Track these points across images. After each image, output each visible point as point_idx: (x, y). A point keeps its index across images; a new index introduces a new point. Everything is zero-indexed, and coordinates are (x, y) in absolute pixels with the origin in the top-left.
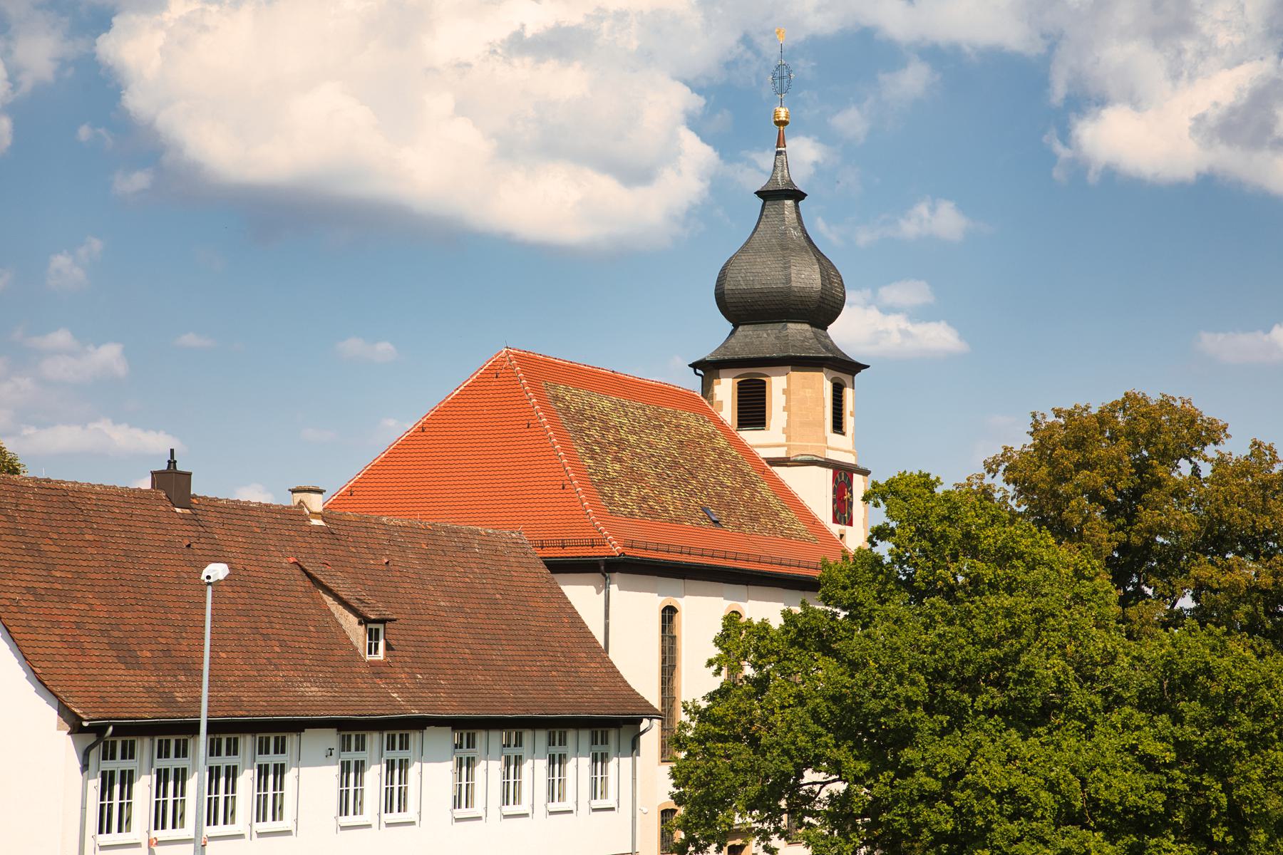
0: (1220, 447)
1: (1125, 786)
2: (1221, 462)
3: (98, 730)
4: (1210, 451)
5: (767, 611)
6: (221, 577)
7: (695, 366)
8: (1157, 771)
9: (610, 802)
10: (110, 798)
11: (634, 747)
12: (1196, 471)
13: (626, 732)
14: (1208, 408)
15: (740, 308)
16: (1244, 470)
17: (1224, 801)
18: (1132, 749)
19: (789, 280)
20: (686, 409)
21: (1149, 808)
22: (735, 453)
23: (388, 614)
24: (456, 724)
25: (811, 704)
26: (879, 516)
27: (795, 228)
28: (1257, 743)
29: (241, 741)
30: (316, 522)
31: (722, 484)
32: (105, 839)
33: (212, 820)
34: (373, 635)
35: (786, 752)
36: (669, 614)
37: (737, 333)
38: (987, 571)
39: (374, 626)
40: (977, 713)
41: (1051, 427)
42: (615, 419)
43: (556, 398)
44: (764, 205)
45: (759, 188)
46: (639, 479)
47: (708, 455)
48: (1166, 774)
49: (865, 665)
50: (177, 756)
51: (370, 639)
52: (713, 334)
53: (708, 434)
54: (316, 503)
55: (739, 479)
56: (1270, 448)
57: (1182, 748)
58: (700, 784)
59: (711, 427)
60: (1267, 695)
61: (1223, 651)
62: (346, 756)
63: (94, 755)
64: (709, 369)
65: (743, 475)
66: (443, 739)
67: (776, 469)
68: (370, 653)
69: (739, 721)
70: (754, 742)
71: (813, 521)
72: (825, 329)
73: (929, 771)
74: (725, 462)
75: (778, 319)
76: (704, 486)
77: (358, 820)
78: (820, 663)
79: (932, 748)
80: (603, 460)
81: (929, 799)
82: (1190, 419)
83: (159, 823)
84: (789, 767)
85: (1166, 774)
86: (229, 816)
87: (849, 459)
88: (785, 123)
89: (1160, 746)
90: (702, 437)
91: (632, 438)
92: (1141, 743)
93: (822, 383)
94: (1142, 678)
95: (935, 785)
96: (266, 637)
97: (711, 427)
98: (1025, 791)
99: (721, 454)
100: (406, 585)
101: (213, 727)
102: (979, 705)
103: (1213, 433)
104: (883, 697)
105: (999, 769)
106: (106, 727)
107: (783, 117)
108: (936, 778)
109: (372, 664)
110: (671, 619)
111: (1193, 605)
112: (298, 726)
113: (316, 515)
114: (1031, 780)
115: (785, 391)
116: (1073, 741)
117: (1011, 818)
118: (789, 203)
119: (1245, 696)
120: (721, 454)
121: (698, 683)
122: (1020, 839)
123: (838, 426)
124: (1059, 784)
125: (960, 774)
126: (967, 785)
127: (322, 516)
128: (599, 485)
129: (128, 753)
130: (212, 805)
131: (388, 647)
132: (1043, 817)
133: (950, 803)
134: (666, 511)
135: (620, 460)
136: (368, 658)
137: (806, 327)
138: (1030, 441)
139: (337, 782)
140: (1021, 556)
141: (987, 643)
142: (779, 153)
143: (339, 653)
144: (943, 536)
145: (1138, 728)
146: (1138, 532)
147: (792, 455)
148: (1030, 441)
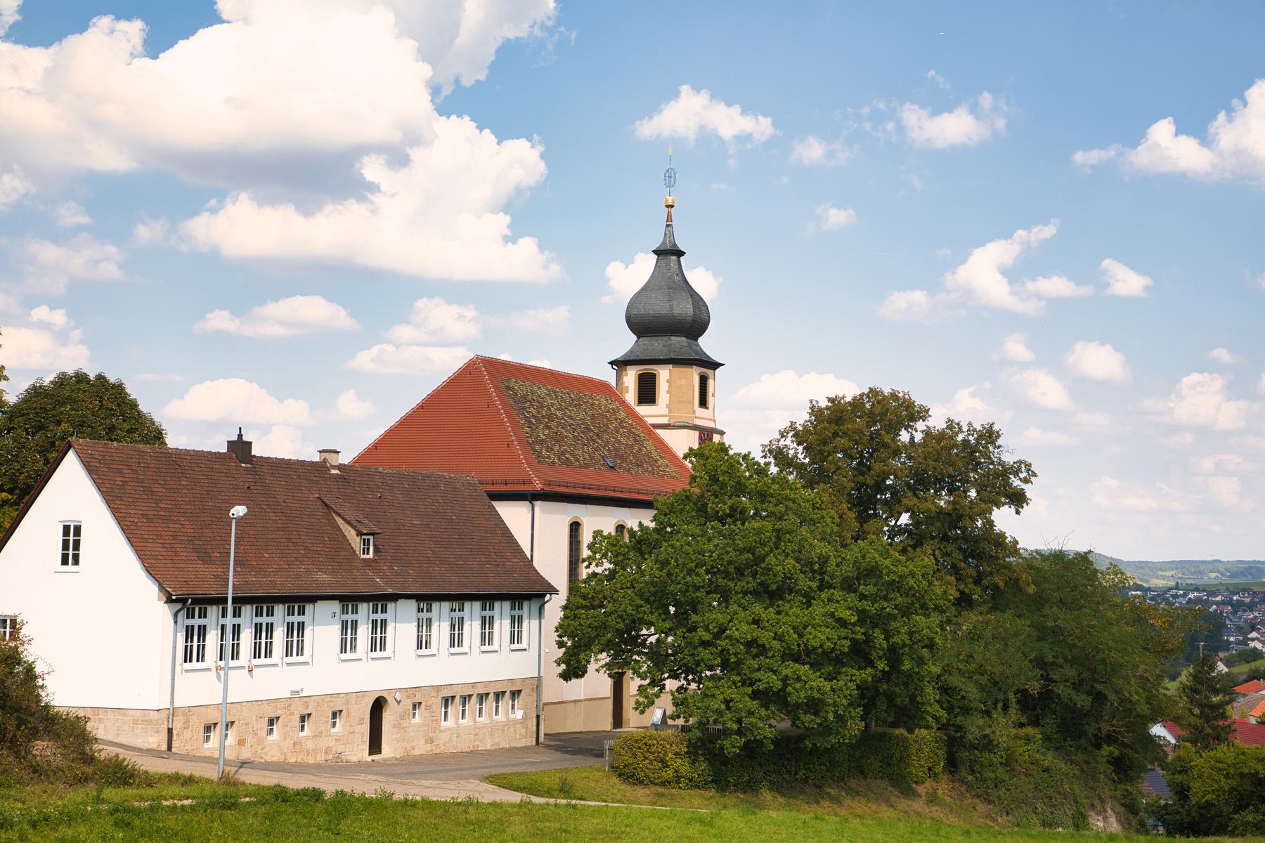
1: (820, 637)
2: (928, 433)
3: (184, 601)
4: (920, 425)
7: (612, 363)
9: (524, 645)
12: (912, 438)
14: (919, 399)
15: (641, 325)
16: (941, 436)
19: (671, 308)
23: (376, 530)
24: (419, 598)
28: (906, 612)
30: (333, 471)
31: (619, 442)
32: (188, 666)
33: (373, 649)
35: (620, 617)
36: (575, 527)
40: (737, 593)
42: (548, 401)
43: (508, 388)
57: (862, 613)
59: (616, 405)
64: (620, 365)
65: (635, 435)
73: (707, 629)
75: (670, 331)
76: (607, 444)
81: (705, 644)
82: (908, 404)
83: (257, 654)
86: (269, 653)
87: (710, 425)
91: (559, 414)
93: (694, 374)
94: (848, 570)
95: (707, 637)
96: (295, 544)
97: (616, 405)
98: (762, 640)
101: (235, 600)
102: (738, 588)
103: (923, 414)
106: (186, 600)
112: (313, 599)
118: (674, 258)
122: (759, 669)
125: (724, 631)
129: (203, 614)
131: (376, 550)
134: (578, 460)
135: (549, 428)
137: (684, 339)
139: (339, 632)
147: (672, 422)
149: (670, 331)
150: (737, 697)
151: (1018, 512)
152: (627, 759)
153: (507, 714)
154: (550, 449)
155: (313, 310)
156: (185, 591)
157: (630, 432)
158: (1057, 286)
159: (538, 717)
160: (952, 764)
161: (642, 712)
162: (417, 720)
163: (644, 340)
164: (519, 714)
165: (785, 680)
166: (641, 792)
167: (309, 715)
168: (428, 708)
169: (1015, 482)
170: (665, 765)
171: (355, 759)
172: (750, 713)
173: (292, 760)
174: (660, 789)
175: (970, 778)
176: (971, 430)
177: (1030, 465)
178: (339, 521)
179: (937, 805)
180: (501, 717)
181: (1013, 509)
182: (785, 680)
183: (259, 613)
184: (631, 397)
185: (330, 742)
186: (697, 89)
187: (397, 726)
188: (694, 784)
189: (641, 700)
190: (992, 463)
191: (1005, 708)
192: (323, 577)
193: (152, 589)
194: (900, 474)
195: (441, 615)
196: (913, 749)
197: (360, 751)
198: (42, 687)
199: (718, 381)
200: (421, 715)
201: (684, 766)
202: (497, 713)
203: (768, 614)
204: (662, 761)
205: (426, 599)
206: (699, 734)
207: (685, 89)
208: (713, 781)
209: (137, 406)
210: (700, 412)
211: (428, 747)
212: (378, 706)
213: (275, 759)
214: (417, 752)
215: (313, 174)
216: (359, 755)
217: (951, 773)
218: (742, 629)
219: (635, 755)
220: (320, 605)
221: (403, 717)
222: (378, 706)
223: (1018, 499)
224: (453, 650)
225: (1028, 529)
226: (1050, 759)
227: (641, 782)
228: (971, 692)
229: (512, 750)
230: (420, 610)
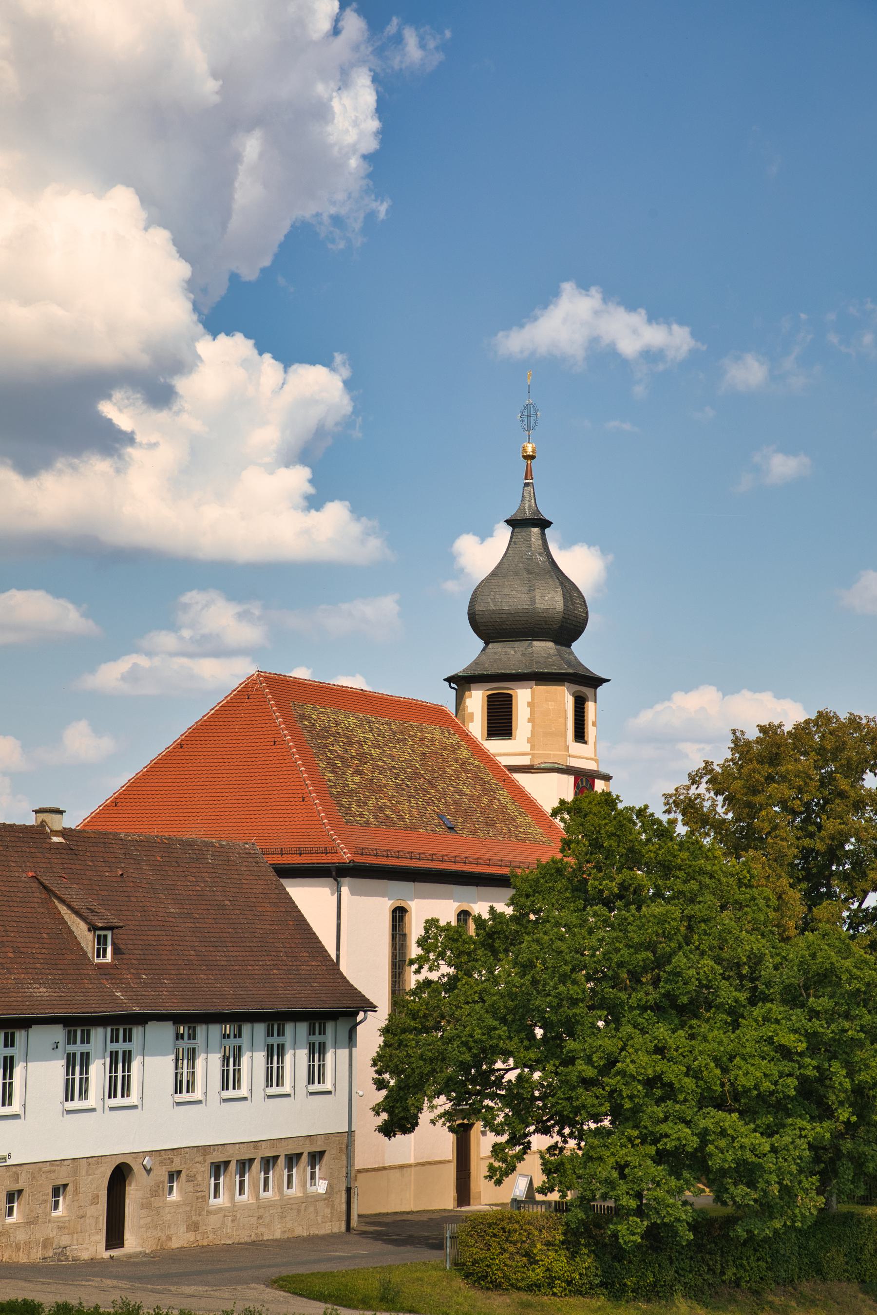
1: (755, 1073)
7: (449, 680)
9: (328, 1086)
11: (351, 1040)
13: (343, 1027)
15: (489, 627)
17: (848, 1085)
18: (770, 1041)
19: (533, 602)
20: (432, 723)
21: (783, 1092)
22: (477, 763)
23: (115, 922)
24: (177, 1019)
27: (540, 554)
30: (55, 839)
31: (461, 793)
33: (112, 1094)
34: (101, 941)
35: (465, 1044)
36: (399, 915)
37: (488, 650)
39: (102, 933)
40: (631, 1008)
42: (360, 735)
43: (303, 717)
44: (512, 533)
45: (508, 518)
47: (451, 765)
48: (798, 1062)
51: (99, 944)
52: (468, 649)
53: (452, 745)
55: (478, 787)
62: (71, 1049)
64: (462, 683)
65: (483, 783)
66: (164, 1032)
68: (98, 956)
69: (431, 1015)
72: (569, 646)
73: (589, 1061)
76: (443, 795)
77: (126, 1102)
80: (344, 773)
81: (587, 1083)
85: (798, 1062)
86: (84, 1093)
87: (590, 766)
88: (532, 457)
89: (793, 1037)
90: (445, 749)
91: (375, 752)
92: (777, 1035)
94: (791, 975)
95: (590, 1072)
99: (464, 763)
100: (138, 894)
102: (633, 1002)
107: (529, 451)
109: (100, 966)
110: (402, 919)
114: (674, 1067)
115: (529, 704)
117: (659, 1101)
118: (536, 530)
119: (865, 993)
123: (580, 735)
124: (702, 1072)
131: (116, 951)
132: (686, 1100)
134: (402, 819)
136: (96, 961)
139: (63, 1071)
142: (527, 485)
143: (70, 957)
146: (822, 839)
147: (536, 763)
150: (634, 1160)
152: (477, 1251)
153: (304, 1185)
154: (362, 804)
157: (476, 778)
159: (349, 1190)
161: (499, 1182)
162: (175, 1196)
164: (321, 1187)
165: (703, 1136)
167: (20, 1192)
168: (191, 1179)
170: (532, 1260)
171: (85, 1256)
174: (526, 1297)
180: (295, 1191)
182: (703, 1136)
184: (477, 727)
185: (50, 1231)
186: (584, 286)
188: (574, 1289)
189: (497, 1164)
192: (41, 991)
197: (93, 1246)
204: (527, 1254)
207: (568, 287)
210: (576, 748)
211: (191, 1237)
212: (120, 1175)
214: (175, 1244)
218: (639, 1062)
219: (488, 1247)
221: (155, 1192)
222: (120, 1175)
224: (227, 1094)
227: (497, 1286)
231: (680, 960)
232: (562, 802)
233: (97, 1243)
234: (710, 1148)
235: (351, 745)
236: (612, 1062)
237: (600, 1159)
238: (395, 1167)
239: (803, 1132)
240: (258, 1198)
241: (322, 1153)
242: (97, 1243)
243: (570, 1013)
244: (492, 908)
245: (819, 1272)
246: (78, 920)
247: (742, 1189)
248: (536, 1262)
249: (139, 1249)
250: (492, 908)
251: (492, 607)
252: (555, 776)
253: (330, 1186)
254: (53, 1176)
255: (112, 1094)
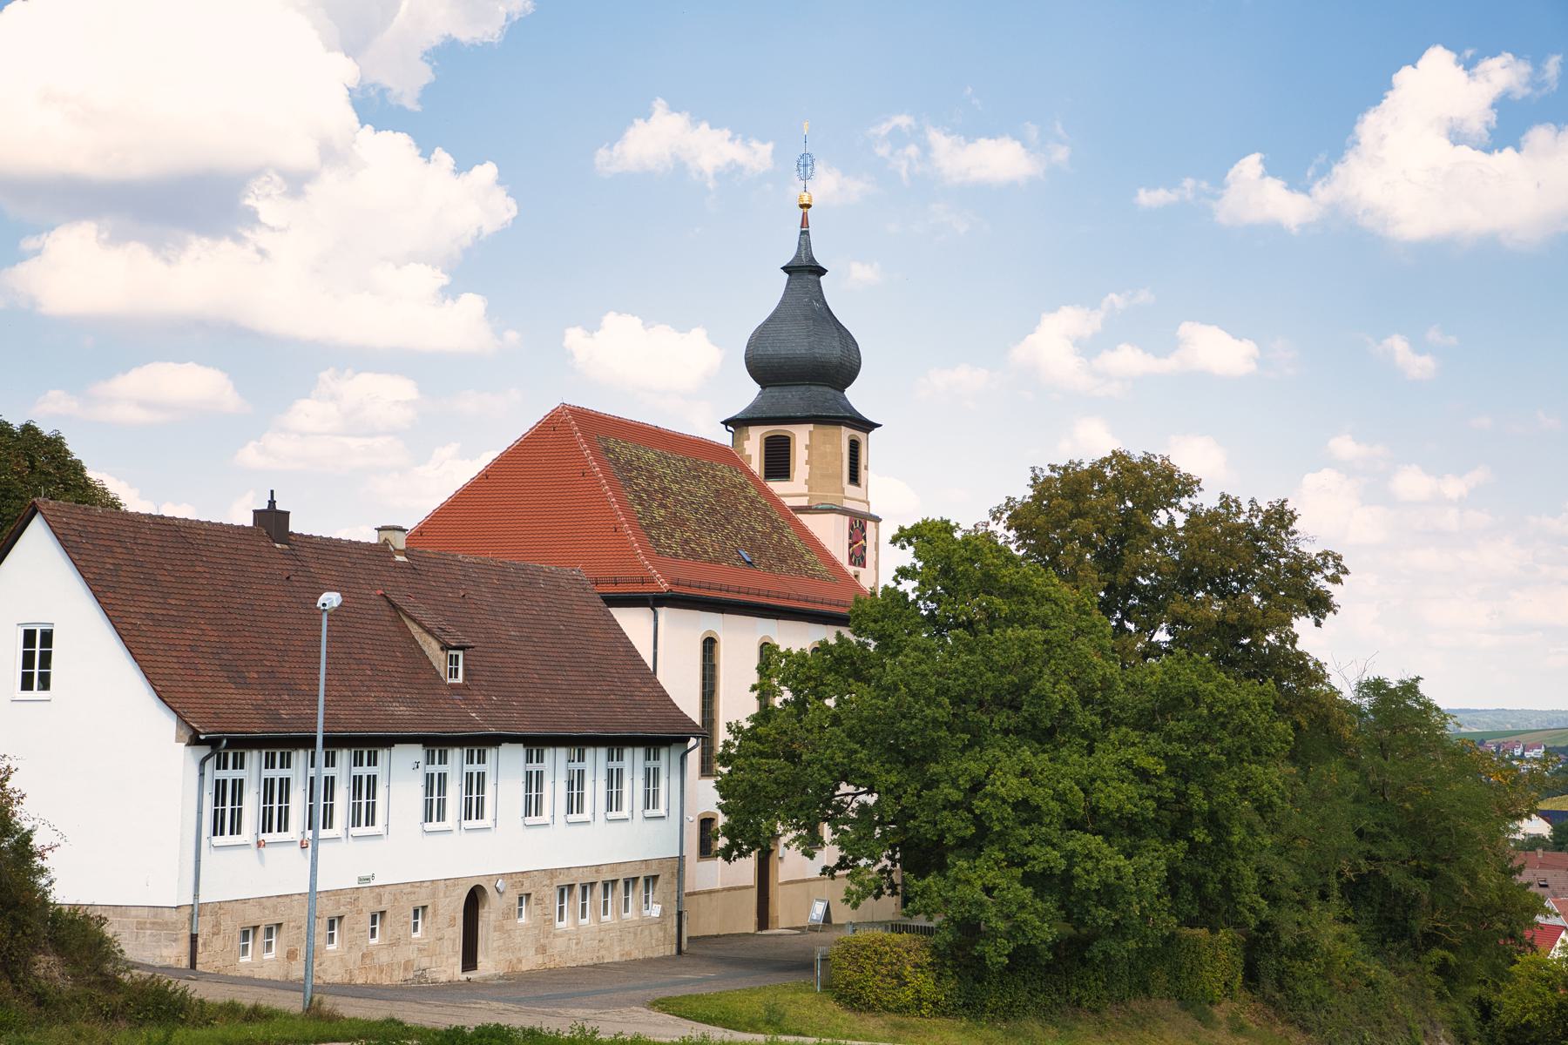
0: (1194, 500)
1: (1119, 796)
2: (1193, 514)
4: (1185, 502)
5: (798, 638)
6: (335, 605)
7: (726, 423)
8: (1148, 782)
9: (662, 811)
10: (223, 804)
12: (1171, 521)
14: (1186, 461)
15: (763, 369)
16: (1213, 517)
23: (467, 642)
25: (847, 724)
26: (906, 557)
28: (1234, 756)
29: (338, 754)
30: (399, 558)
31: (753, 529)
32: (218, 840)
35: (826, 767)
36: (709, 645)
38: (1003, 606)
39: (454, 653)
40: (995, 732)
41: (1048, 480)
43: (607, 450)
46: (681, 523)
49: (897, 689)
50: (235, 767)
54: (399, 541)
56: (1235, 501)
58: (744, 797)
59: (742, 478)
60: (1246, 716)
61: (1208, 677)
62: (431, 769)
63: (210, 764)
64: (736, 424)
65: (772, 521)
67: (800, 516)
70: (792, 757)
71: (833, 563)
73: (954, 783)
74: (756, 509)
75: (805, 373)
76: (739, 531)
78: (854, 688)
79: (955, 764)
81: (953, 806)
83: (267, 827)
84: (828, 780)
86: (441, 817)
87: (861, 508)
88: (809, 206)
89: (1152, 760)
91: (675, 487)
93: (846, 433)
95: (956, 796)
103: (1188, 486)
104: (914, 717)
105: (1015, 781)
106: (219, 741)
108: (958, 788)
109: (451, 685)
111: (1168, 638)
112: (389, 742)
113: (400, 552)
115: (807, 447)
116: (1076, 756)
120: (752, 502)
121: (737, 704)
122: (1031, 843)
126: (986, 795)
127: (404, 553)
128: (646, 528)
130: (356, 809)
133: (971, 811)
134: (706, 552)
136: (449, 681)
138: (1030, 492)
140: (1033, 594)
141: (1005, 670)
144: (965, 574)
145: (1134, 744)
147: (814, 504)
148: (1030, 492)
149: (805, 373)
150: (1003, 883)
151: (1318, 624)
152: (850, 973)
153: (640, 910)
154: (670, 536)
155: (191, 383)
156: (217, 727)
157: (766, 517)
158: (1128, 359)
159: (680, 914)
160: (1252, 976)
161: (855, 906)
162: (523, 920)
163: (775, 392)
164: (655, 911)
165: (1070, 856)
166: (871, 1023)
167: (340, 918)
168: (539, 901)
169: (1319, 580)
170: (902, 982)
171: (443, 978)
172: (1022, 907)
173: (360, 981)
174: (897, 1018)
175: (1278, 996)
176: (1255, 508)
177: (1340, 558)
178: (414, 629)
179: (1245, 1036)
180: (631, 915)
181: (1311, 620)
182: (1070, 856)
183: (358, 762)
184: (756, 465)
185: (410, 953)
186: (674, 108)
187: (500, 928)
188: (940, 1010)
189: (854, 887)
190: (1285, 556)
191: (1323, 896)
192: (401, 710)
193: (164, 723)
194: (1165, 568)
195: (556, 762)
196: (1206, 958)
197: (449, 968)
198: (42, 871)
199: (873, 444)
200: (529, 913)
201: (925, 983)
202: (626, 910)
203: (1041, 762)
204: (898, 977)
205: (535, 743)
206: (949, 938)
207: (660, 105)
208: (964, 1005)
209: (82, 469)
210: (850, 490)
211: (540, 959)
212: (474, 899)
213: (337, 979)
214: (525, 967)
215: (190, 203)
216: (449, 972)
217: (1250, 989)
218: (1008, 785)
219: (862, 969)
220: (398, 750)
221: (506, 916)
222: (474, 899)
223: (1319, 605)
224: (611, 815)
225: (1344, 650)
226: (1374, 969)
227: (871, 1008)
228: (1289, 874)
229: (648, 962)
230: (529, 760)
231: (1045, 683)
232: (902, 529)
233: (454, 965)
234: (1077, 870)
235: (653, 479)
236: (977, 787)
237: (968, 882)
238: (704, 893)
239: (1156, 858)
240: (599, 921)
241: (655, 878)
242: (454, 965)
243: (935, 735)
244: (839, 633)
245: (1146, 990)
246: (430, 639)
247: (1102, 912)
248: (906, 984)
249: (493, 972)
250: (839, 633)
251: (770, 351)
252: (833, 516)
253: (663, 909)
254: (413, 897)
255: (468, 816)
